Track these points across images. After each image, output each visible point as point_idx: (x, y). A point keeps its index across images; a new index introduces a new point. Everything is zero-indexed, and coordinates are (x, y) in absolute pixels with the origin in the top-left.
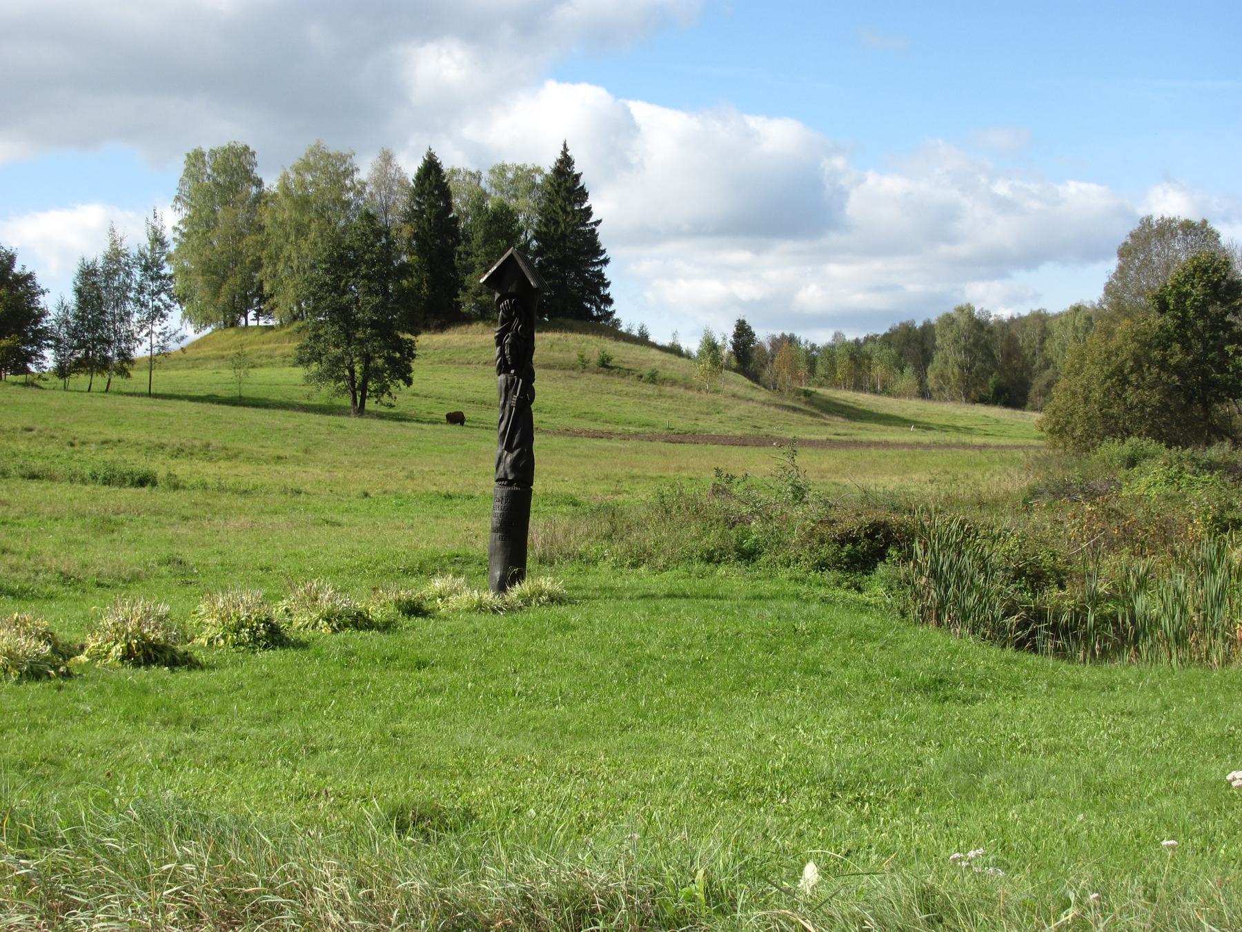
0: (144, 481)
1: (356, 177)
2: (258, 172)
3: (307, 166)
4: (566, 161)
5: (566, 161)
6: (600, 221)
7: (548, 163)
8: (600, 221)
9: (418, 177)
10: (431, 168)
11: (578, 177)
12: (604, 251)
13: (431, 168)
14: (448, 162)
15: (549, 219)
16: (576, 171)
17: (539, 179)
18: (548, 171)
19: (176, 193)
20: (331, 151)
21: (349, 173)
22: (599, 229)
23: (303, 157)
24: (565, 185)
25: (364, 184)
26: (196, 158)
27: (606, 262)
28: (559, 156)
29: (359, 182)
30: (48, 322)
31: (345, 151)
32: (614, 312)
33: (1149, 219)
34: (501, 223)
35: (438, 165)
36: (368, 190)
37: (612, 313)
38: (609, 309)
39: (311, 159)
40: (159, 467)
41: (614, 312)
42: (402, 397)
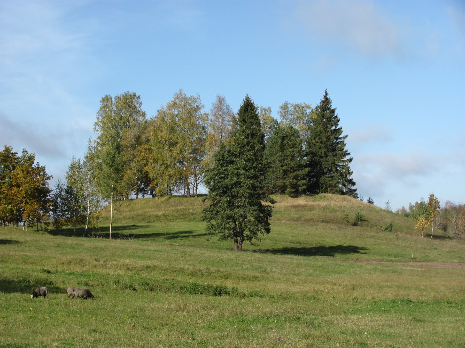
0: (219, 292)
1: (203, 111)
2: (143, 108)
3: (174, 105)
4: (326, 101)
5: (326, 101)
6: (346, 137)
7: (315, 102)
8: (346, 137)
9: (240, 111)
10: (248, 107)
11: (333, 111)
12: (349, 154)
13: (248, 107)
14: (258, 102)
15: (316, 134)
16: (333, 108)
17: (308, 111)
18: (314, 107)
19: (96, 121)
20: (188, 96)
21: (196, 109)
22: (346, 141)
23: (173, 100)
24: (326, 115)
25: (207, 115)
26: (106, 99)
27: (350, 160)
28: (323, 99)
29: (205, 114)
30: (51, 196)
31: (196, 96)
32: (356, 190)
33: (238, 113)
34: (286, 138)
35: (252, 104)
36: (210, 118)
37: (355, 190)
38: (352, 188)
39: (177, 101)
40: (229, 284)
41: (356, 190)
42: (265, 240)
